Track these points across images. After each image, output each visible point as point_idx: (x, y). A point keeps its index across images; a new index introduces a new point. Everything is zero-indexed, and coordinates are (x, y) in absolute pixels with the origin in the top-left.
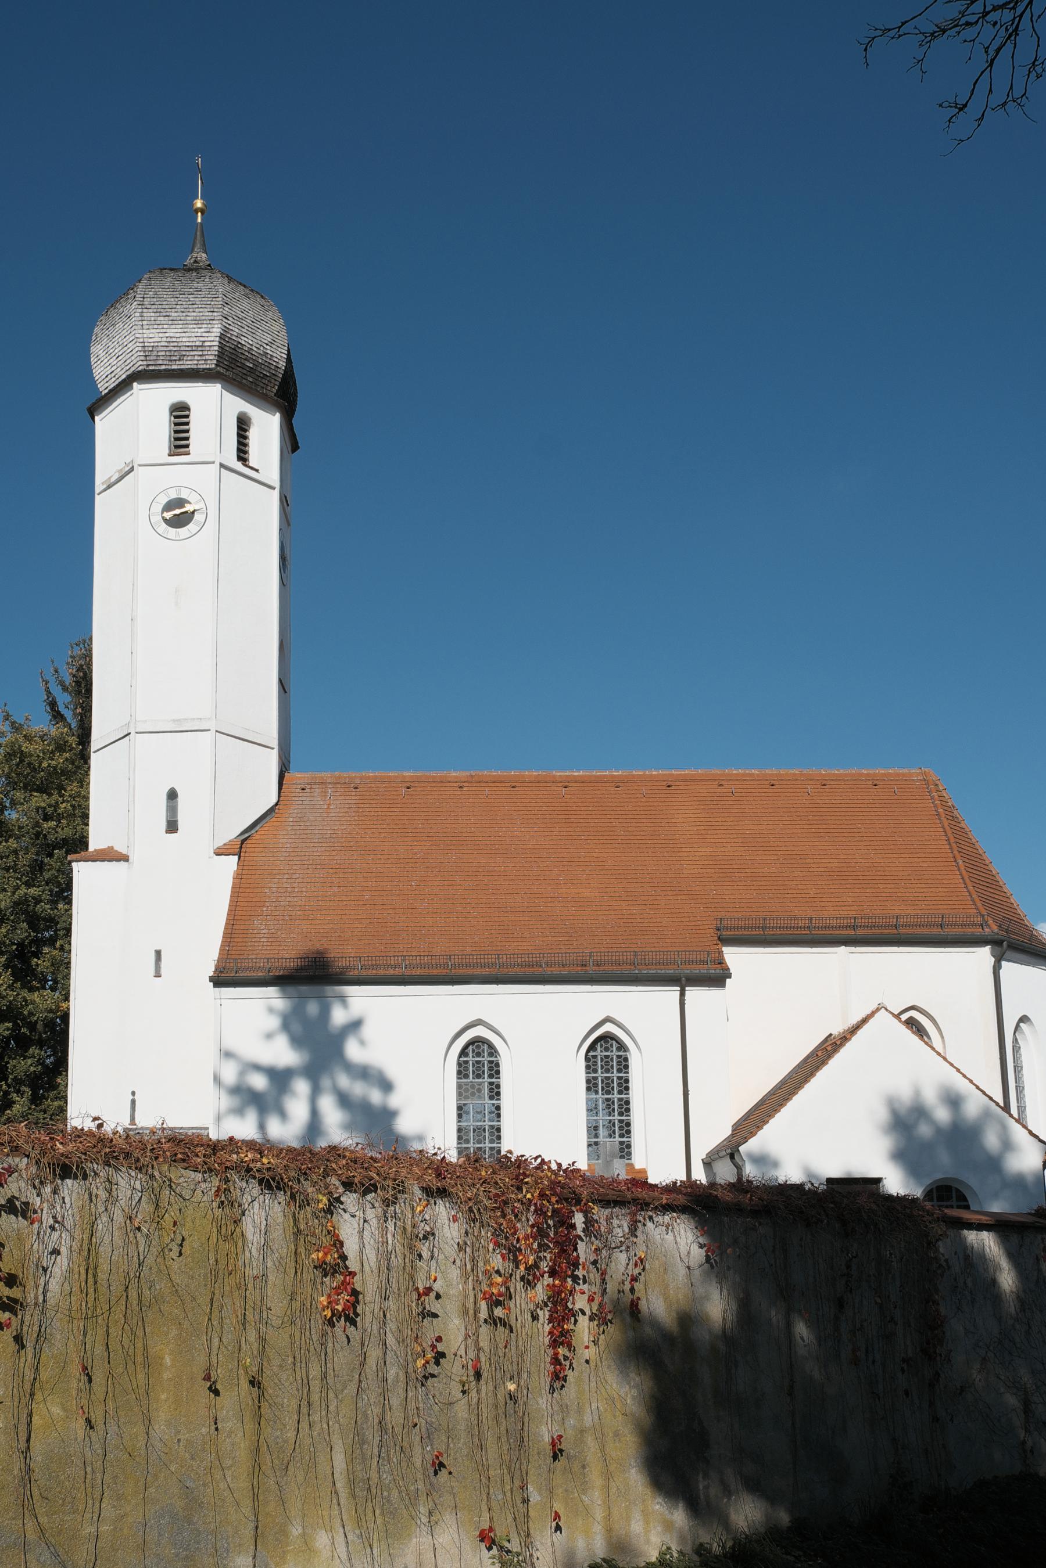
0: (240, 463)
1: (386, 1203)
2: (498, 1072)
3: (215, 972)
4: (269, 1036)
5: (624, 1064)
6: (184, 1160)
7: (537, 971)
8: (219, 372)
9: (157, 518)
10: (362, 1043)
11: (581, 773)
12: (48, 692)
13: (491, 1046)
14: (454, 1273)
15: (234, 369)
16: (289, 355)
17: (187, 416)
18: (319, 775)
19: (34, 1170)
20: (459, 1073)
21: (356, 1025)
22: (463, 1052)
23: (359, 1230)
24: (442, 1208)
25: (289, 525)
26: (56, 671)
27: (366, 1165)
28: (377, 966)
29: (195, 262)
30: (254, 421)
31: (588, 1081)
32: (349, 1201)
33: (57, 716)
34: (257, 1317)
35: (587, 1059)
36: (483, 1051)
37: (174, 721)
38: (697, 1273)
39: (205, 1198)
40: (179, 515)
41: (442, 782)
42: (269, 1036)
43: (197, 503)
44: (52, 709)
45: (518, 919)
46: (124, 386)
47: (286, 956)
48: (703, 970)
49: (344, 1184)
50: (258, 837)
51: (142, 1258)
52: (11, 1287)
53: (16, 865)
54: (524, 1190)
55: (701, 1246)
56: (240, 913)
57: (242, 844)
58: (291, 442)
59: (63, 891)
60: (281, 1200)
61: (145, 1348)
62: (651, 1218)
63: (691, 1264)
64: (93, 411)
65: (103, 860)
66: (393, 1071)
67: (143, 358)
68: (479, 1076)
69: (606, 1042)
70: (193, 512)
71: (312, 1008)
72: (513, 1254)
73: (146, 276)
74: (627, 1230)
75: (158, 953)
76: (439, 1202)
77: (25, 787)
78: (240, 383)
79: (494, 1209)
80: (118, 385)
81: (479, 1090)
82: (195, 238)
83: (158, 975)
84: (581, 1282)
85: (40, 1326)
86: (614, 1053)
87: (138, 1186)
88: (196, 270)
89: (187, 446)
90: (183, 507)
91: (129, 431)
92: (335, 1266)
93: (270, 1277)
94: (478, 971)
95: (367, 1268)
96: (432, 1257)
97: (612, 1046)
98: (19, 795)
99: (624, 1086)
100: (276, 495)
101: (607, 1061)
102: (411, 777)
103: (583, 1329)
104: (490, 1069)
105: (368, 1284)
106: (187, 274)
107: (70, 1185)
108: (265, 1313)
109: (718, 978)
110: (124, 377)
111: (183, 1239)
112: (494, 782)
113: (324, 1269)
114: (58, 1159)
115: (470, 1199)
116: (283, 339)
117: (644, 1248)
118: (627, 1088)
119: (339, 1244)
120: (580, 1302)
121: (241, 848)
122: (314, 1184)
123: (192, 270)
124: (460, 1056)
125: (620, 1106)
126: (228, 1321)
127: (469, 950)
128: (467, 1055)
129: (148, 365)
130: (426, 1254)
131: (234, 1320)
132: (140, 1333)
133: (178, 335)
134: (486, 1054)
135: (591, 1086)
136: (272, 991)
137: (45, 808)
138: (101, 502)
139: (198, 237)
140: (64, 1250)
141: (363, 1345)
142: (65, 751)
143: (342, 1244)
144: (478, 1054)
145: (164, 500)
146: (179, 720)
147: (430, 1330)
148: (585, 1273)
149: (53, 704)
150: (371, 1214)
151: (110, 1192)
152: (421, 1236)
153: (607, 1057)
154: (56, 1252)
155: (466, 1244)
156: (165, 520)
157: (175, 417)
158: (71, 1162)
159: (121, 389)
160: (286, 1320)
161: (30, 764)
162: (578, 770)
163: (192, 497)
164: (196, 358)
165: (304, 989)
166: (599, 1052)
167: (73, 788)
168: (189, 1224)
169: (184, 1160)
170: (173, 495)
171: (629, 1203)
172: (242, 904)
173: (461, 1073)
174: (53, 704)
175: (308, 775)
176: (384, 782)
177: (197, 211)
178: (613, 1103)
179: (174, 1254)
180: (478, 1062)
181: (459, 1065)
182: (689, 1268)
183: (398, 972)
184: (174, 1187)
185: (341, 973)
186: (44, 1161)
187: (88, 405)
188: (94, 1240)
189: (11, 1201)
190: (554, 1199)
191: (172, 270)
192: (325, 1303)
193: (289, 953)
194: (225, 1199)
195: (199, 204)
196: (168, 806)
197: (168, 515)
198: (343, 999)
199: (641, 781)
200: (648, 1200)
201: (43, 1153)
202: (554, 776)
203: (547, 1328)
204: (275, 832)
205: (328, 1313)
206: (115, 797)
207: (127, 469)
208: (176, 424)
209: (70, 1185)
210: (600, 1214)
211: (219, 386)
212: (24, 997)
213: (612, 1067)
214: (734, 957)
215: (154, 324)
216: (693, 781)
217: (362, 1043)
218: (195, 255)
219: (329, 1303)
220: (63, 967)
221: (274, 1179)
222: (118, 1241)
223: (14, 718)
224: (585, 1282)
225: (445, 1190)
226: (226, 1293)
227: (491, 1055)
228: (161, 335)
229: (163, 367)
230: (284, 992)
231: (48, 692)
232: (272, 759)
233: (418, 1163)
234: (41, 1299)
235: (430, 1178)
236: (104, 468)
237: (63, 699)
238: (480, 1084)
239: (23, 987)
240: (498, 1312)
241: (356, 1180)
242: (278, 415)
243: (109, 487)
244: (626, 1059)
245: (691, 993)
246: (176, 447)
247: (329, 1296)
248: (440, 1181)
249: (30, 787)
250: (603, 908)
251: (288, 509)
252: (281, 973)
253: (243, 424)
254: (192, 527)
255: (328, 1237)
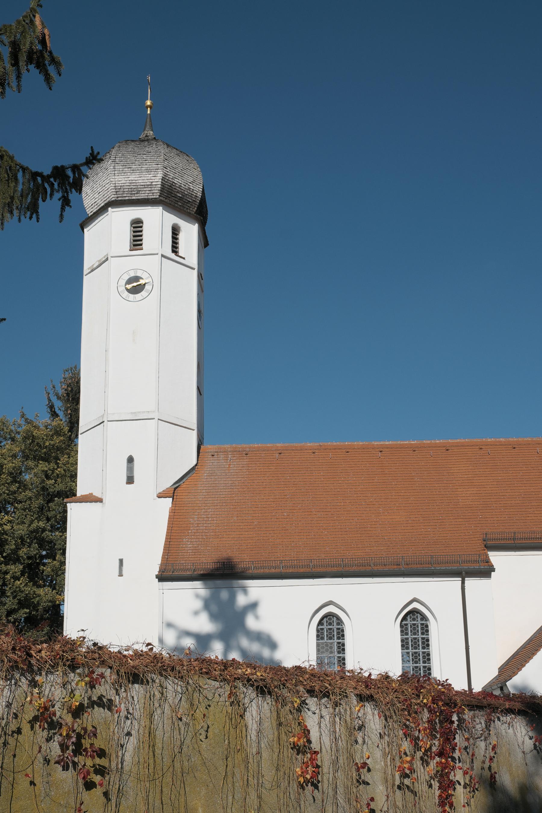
0: (173, 254)
1: (336, 704)
2: (343, 636)
3: (159, 572)
4: (196, 613)
5: (425, 629)
6: (207, 673)
7: (368, 569)
8: (161, 200)
9: (122, 289)
10: (257, 617)
11: (390, 443)
12: (49, 400)
13: (338, 618)
14: (378, 754)
15: (170, 198)
16: (203, 189)
17: (141, 227)
18: (223, 446)
19: (114, 677)
20: (318, 636)
21: (253, 606)
22: (320, 623)
23: (318, 721)
24: (369, 709)
25: (203, 291)
26: (54, 387)
27: (322, 678)
28: (264, 567)
29: (146, 136)
30: (182, 229)
31: (402, 641)
32: (311, 703)
33: (54, 415)
34: (256, 781)
35: (401, 626)
36: (333, 622)
37: (132, 413)
38: (529, 756)
39: (221, 699)
40: (136, 287)
41: (301, 450)
42: (196, 613)
43: (147, 279)
44: (51, 411)
45: (354, 536)
46: (103, 210)
47: (205, 561)
48: (476, 566)
49: (309, 692)
50: (184, 486)
51: (182, 739)
52: (101, 758)
53: (30, 507)
54: (421, 697)
55: (531, 738)
56: (174, 534)
57: (174, 490)
58: (204, 241)
59: (61, 524)
60: (269, 701)
61: (186, 801)
62: (499, 719)
63: (525, 750)
64: (82, 227)
65: (87, 502)
66: (277, 636)
67: (114, 193)
68: (330, 638)
69: (414, 615)
70: (145, 285)
71: (224, 595)
72: (415, 741)
73: (117, 145)
74: (484, 725)
75: (121, 561)
76: (367, 704)
77: (34, 458)
78: (174, 206)
79: (403, 710)
80: (99, 210)
81: (331, 648)
82: (146, 122)
83: (121, 575)
84: (457, 762)
85: (120, 786)
86: (419, 622)
87: (179, 689)
88: (148, 140)
89: (141, 245)
90: (139, 281)
91: (105, 237)
92: (303, 748)
93: (263, 754)
94: (329, 570)
95: (324, 749)
96: (364, 742)
97: (417, 617)
98: (31, 463)
99: (426, 643)
100: (195, 273)
101: (414, 626)
102: (282, 446)
103: (460, 794)
104: (338, 633)
105: (325, 760)
106: (142, 143)
107: (137, 688)
108: (261, 779)
109: (486, 571)
110: (103, 205)
111: (208, 727)
112: (335, 449)
113: (298, 750)
114: (130, 670)
115: (388, 703)
116: (200, 179)
117: (495, 738)
118: (428, 645)
119: (306, 732)
120: (458, 776)
121: (174, 493)
122: (290, 690)
123: (145, 141)
124: (318, 625)
125: (424, 657)
126: (237, 784)
127: (323, 556)
128: (323, 624)
129: (118, 197)
130: (360, 740)
131: (241, 784)
132: (182, 792)
133: (136, 179)
134: (335, 624)
135: (404, 644)
136: (198, 584)
137: (47, 471)
138: (87, 280)
139: (148, 122)
140: (133, 732)
141: (323, 801)
142: (60, 435)
143: (309, 731)
144: (330, 624)
145: (126, 277)
146: (135, 413)
147: (365, 793)
148: (459, 754)
149: (52, 407)
150: (325, 712)
151: (162, 694)
152: (356, 727)
153: (414, 624)
154: (129, 734)
155: (385, 734)
156: (127, 290)
157: (134, 227)
158: (139, 672)
159: (101, 212)
160: (274, 784)
161: (38, 443)
162: (388, 441)
163: (144, 275)
164: (147, 192)
165: (219, 582)
166: (409, 622)
167: (64, 459)
168: (211, 717)
169: (207, 673)
170: (132, 274)
171: (486, 707)
172: (175, 529)
173: (319, 636)
174: (52, 407)
175: (216, 446)
176: (264, 450)
177: (147, 107)
178: (419, 655)
179: (203, 737)
180: (330, 629)
181: (318, 631)
182: (524, 752)
183: (277, 571)
184: (202, 691)
185: (243, 572)
186: (122, 671)
187: (80, 222)
188: (152, 726)
189: (100, 698)
190: (440, 703)
191: (132, 141)
192: (300, 773)
193: (208, 560)
194: (235, 701)
195: (149, 103)
196: (128, 467)
197: (129, 287)
198: (244, 589)
199: (429, 447)
200: (497, 705)
201: (121, 665)
202: (373, 445)
203: (438, 793)
204: (195, 483)
205: (301, 780)
206: (94, 461)
207: (104, 259)
208: (134, 232)
209: (137, 688)
210: (468, 715)
211: (161, 208)
212: (34, 592)
213: (418, 631)
214: (495, 557)
215: (123, 172)
216: (463, 446)
217: (257, 617)
218: (146, 132)
219: (302, 773)
220: (60, 571)
221: (266, 687)
222: (167, 728)
223: (27, 416)
224: (460, 762)
225: (372, 696)
226: (236, 765)
227: (338, 624)
228: (126, 179)
229: (127, 198)
230: (205, 584)
231: (49, 400)
232: (194, 436)
233: (352, 677)
234: (120, 766)
235: (361, 688)
236: (90, 259)
237: (58, 404)
238: (332, 643)
239: (34, 585)
240: (407, 781)
241: (317, 689)
242: (197, 225)
243: (92, 271)
244: (427, 626)
245: (470, 582)
246: (134, 245)
247: (302, 768)
248: (370, 690)
249: (37, 458)
250: (408, 528)
251: (202, 281)
252: (202, 572)
253: (175, 231)
254: (144, 293)
255: (299, 727)
